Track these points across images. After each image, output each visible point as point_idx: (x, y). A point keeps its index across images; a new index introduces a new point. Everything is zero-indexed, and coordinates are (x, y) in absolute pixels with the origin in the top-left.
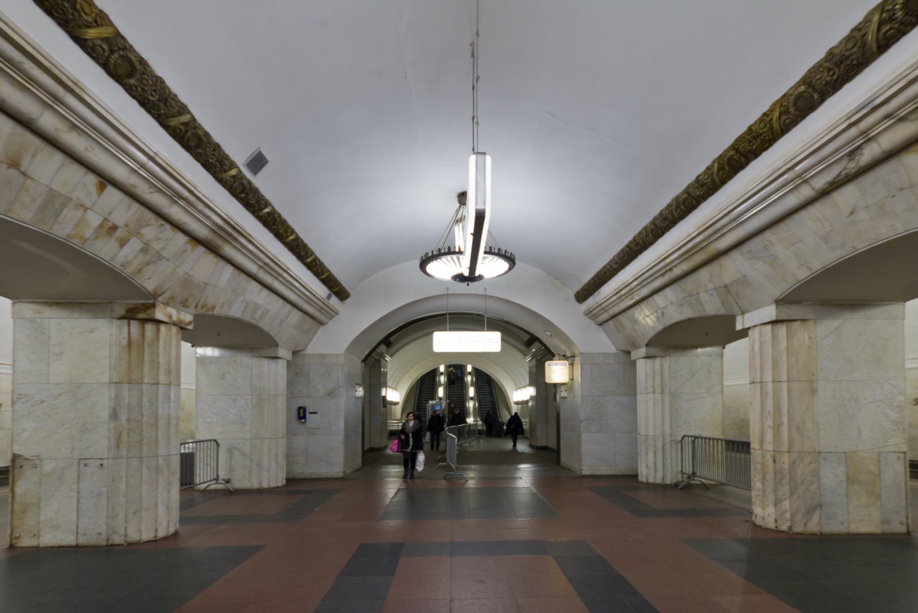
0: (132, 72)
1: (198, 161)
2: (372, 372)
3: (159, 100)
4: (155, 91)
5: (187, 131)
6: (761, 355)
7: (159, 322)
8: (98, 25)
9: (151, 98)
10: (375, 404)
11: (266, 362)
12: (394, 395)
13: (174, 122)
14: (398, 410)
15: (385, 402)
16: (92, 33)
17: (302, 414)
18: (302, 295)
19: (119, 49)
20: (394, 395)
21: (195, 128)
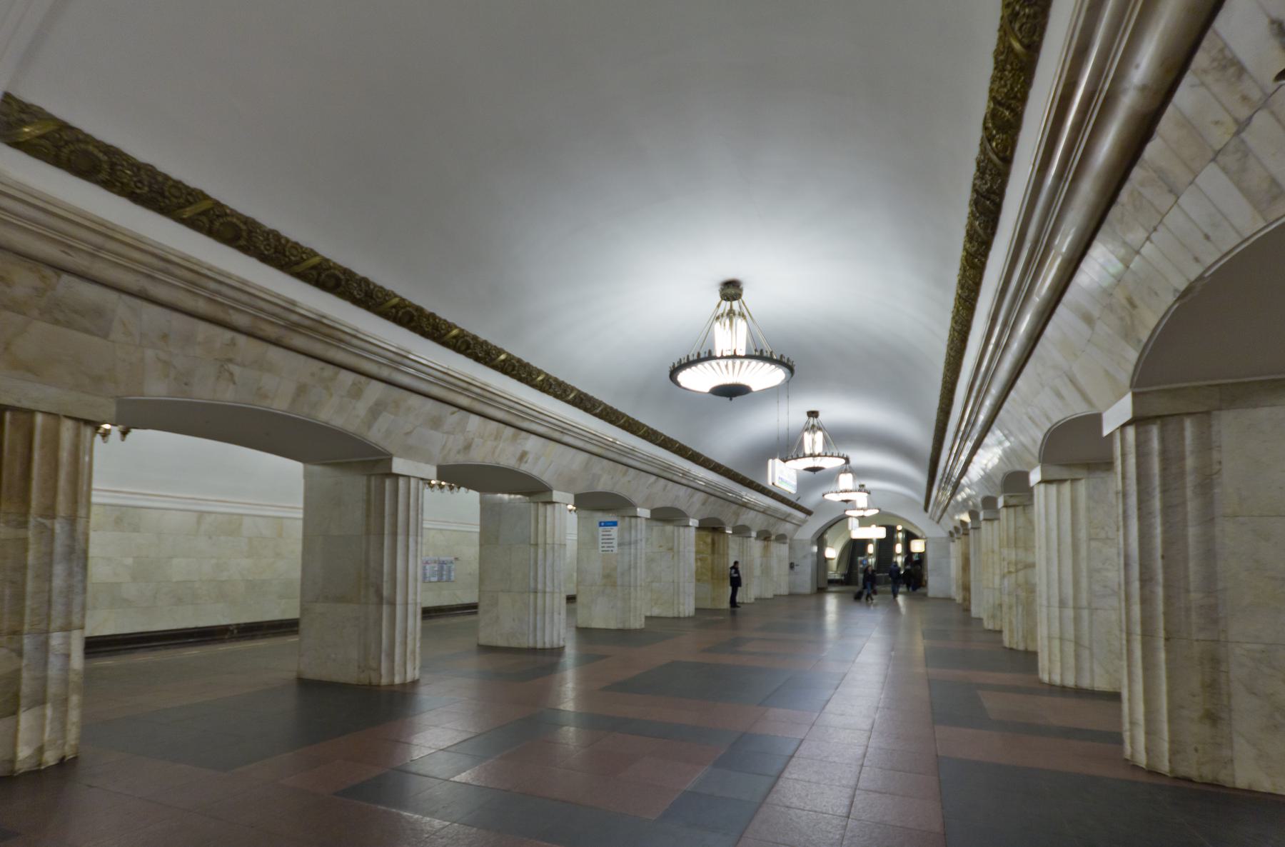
0: (411, 318)
1: (251, 255)
2: (821, 541)
3: (276, 252)
4: (140, 181)
5: (319, 275)
6: (1059, 551)
7: (397, 476)
8: (191, 204)
9: (138, 191)
10: (822, 561)
11: (682, 529)
12: (832, 553)
13: (298, 269)
14: (834, 564)
15: (826, 560)
16: (188, 213)
17: (792, 566)
18: (438, 382)
19: (67, 143)
20: (832, 553)
21: (406, 306)
